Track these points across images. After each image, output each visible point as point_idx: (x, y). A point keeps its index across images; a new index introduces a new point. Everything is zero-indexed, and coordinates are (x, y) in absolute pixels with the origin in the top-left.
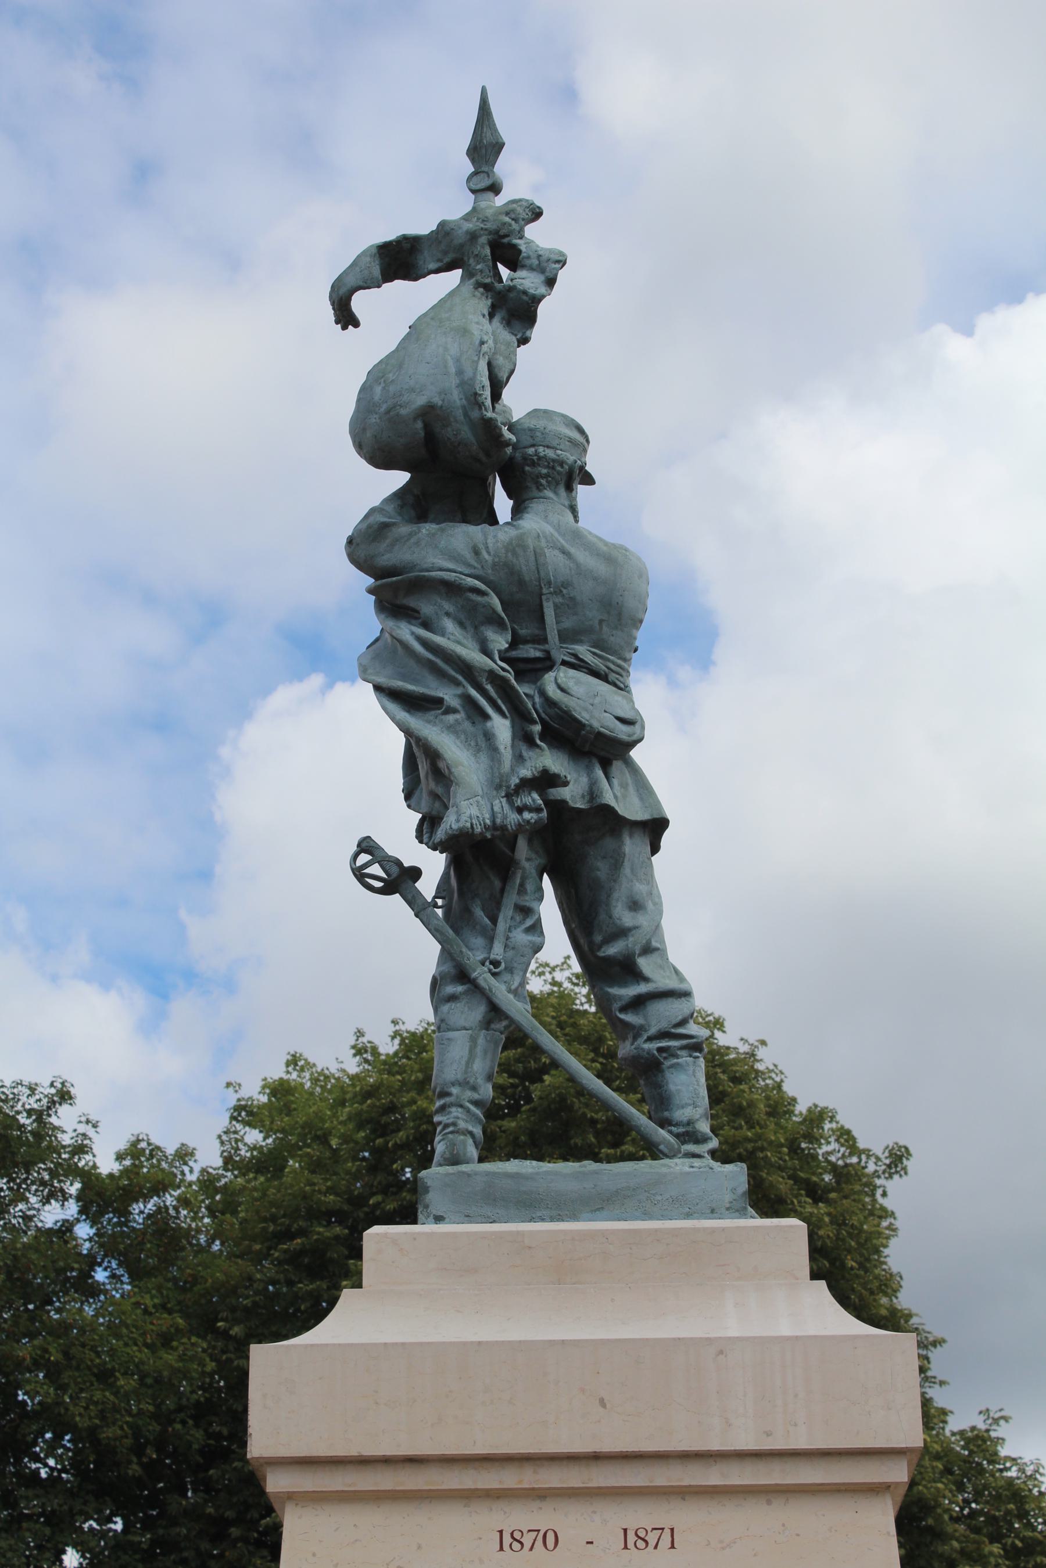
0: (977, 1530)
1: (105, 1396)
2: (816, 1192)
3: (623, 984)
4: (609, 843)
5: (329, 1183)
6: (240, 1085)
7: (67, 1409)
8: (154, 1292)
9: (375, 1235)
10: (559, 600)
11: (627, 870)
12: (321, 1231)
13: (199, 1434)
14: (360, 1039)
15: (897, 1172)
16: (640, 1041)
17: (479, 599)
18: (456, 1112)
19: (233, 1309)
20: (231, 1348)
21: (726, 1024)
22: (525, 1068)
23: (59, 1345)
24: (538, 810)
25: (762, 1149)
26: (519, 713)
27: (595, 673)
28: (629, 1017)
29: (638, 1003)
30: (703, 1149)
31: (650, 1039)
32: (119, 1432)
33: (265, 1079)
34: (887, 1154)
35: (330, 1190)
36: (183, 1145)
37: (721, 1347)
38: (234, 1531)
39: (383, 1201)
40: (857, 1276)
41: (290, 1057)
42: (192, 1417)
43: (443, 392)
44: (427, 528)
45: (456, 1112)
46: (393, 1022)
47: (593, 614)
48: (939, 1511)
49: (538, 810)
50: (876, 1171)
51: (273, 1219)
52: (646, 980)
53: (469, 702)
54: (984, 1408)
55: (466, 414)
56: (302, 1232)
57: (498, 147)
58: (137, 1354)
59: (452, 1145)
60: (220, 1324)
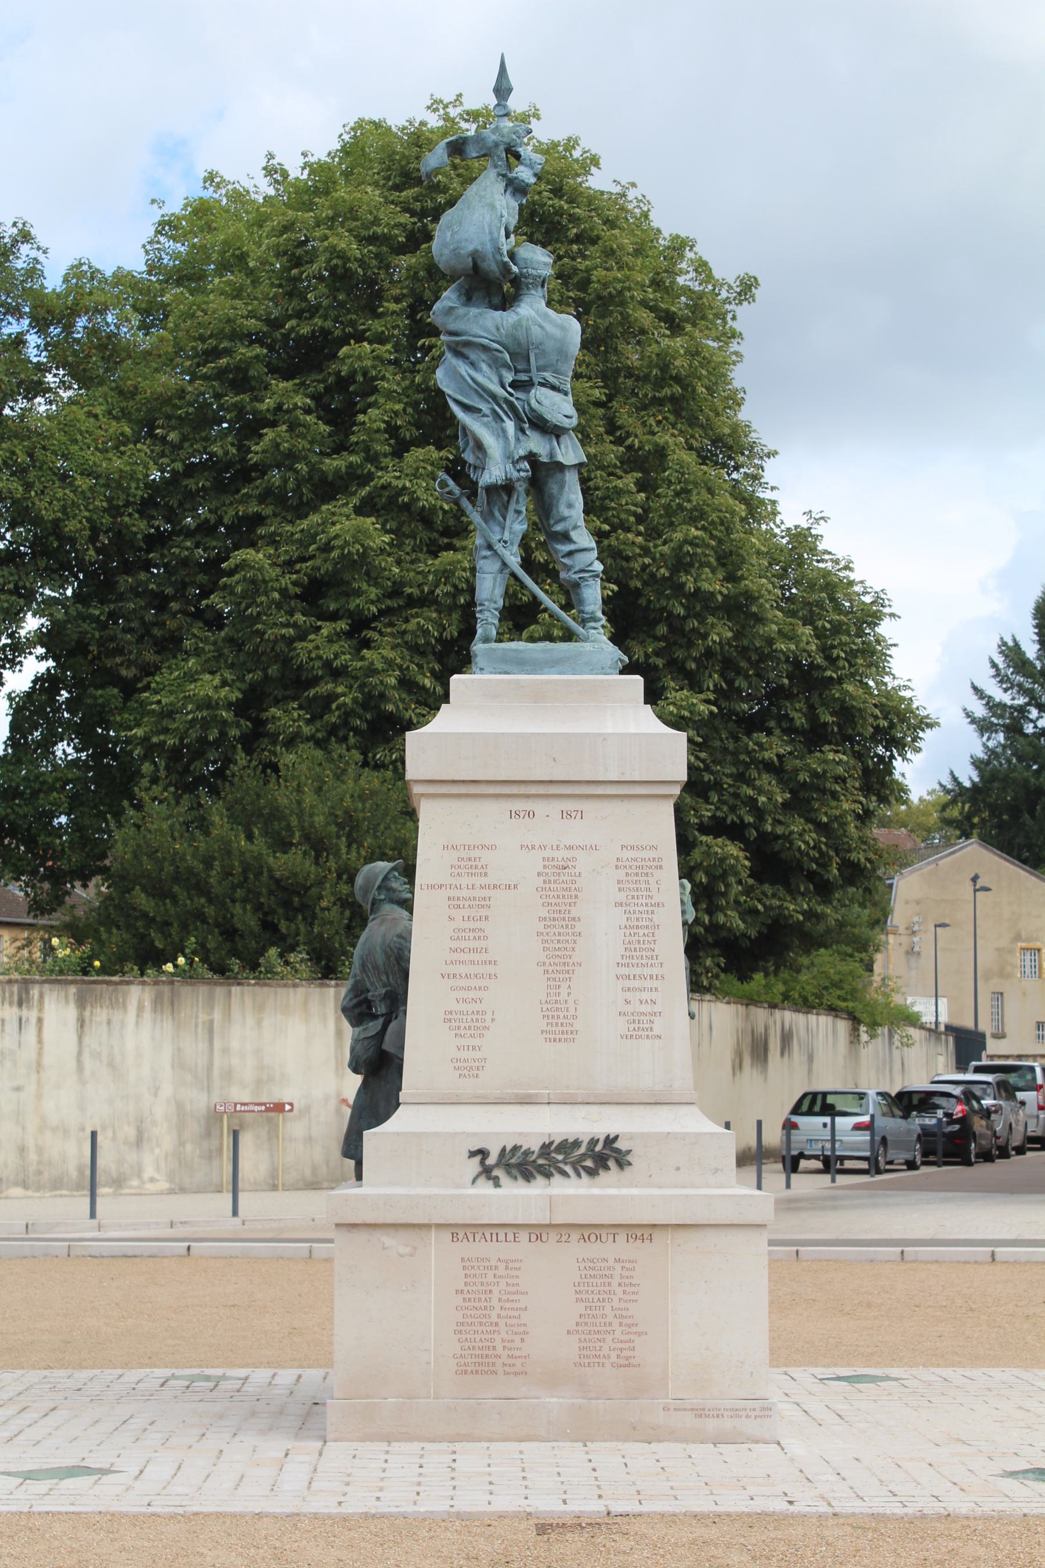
0: (793, 614)
1: (65, 494)
2: (674, 320)
3: (563, 543)
4: (559, 476)
5: (250, 308)
6: (164, 202)
7: (34, 504)
8: (101, 400)
9: (455, 678)
10: (537, 351)
11: (566, 488)
12: (245, 352)
13: (143, 525)
14: (271, 162)
15: (746, 299)
16: (570, 573)
17: (499, 354)
18: (487, 614)
19: (169, 417)
20: (167, 452)
21: (601, 161)
22: (422, 207)
23: (24, 447)
24: (527, 471)
25: (629, 289)
26: (518, 418)
27: (554, 388)
28: (565, 561)
29: (570, 554)
30: (598, 625)
31: (575, 573)
32: (79, 525)
33: (187, 198)
34: (738, 283)
35: (251, 315)
36: (119, 268)
37: (605, 737)
38: (174, 606)
39: (298, 325)
40: (706, 400)
41: (206, 174)
42: (138, 511)
43: (483, 244)
44: (474, 311)
45: (487, 614)
46: (302, 154)
47: (553, 357)
48: (761, 600)
49: (527, 471)
50: (728, 298)
51: (202, 339)
52: (574, 543)
53: (494, 411)
54: (807, 510)
55: (494, 256)
56: (227, 352)
57: (510, 90)
58: (91, 457)
59: (485, 630)
60: (157, 431)
